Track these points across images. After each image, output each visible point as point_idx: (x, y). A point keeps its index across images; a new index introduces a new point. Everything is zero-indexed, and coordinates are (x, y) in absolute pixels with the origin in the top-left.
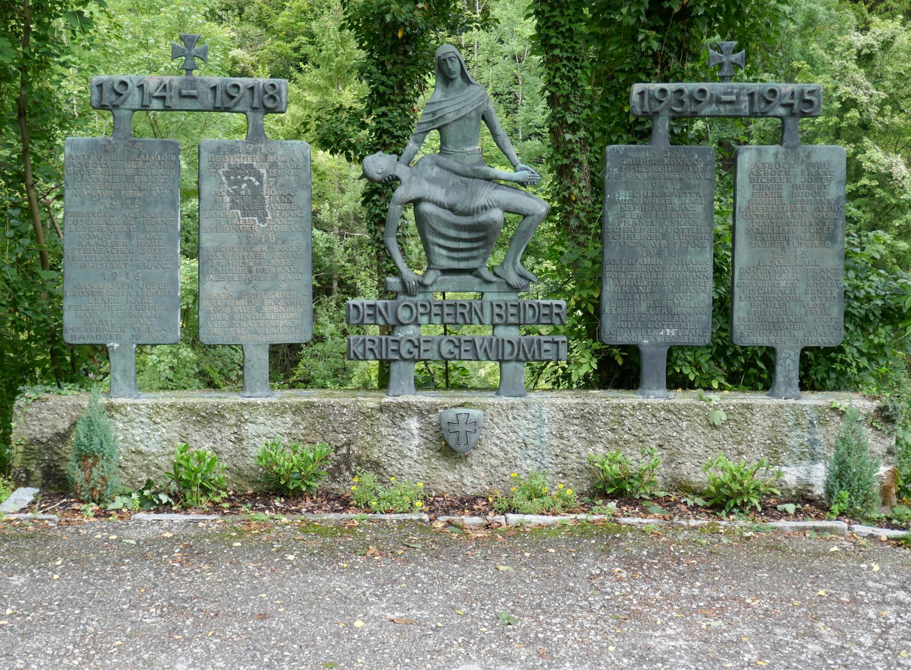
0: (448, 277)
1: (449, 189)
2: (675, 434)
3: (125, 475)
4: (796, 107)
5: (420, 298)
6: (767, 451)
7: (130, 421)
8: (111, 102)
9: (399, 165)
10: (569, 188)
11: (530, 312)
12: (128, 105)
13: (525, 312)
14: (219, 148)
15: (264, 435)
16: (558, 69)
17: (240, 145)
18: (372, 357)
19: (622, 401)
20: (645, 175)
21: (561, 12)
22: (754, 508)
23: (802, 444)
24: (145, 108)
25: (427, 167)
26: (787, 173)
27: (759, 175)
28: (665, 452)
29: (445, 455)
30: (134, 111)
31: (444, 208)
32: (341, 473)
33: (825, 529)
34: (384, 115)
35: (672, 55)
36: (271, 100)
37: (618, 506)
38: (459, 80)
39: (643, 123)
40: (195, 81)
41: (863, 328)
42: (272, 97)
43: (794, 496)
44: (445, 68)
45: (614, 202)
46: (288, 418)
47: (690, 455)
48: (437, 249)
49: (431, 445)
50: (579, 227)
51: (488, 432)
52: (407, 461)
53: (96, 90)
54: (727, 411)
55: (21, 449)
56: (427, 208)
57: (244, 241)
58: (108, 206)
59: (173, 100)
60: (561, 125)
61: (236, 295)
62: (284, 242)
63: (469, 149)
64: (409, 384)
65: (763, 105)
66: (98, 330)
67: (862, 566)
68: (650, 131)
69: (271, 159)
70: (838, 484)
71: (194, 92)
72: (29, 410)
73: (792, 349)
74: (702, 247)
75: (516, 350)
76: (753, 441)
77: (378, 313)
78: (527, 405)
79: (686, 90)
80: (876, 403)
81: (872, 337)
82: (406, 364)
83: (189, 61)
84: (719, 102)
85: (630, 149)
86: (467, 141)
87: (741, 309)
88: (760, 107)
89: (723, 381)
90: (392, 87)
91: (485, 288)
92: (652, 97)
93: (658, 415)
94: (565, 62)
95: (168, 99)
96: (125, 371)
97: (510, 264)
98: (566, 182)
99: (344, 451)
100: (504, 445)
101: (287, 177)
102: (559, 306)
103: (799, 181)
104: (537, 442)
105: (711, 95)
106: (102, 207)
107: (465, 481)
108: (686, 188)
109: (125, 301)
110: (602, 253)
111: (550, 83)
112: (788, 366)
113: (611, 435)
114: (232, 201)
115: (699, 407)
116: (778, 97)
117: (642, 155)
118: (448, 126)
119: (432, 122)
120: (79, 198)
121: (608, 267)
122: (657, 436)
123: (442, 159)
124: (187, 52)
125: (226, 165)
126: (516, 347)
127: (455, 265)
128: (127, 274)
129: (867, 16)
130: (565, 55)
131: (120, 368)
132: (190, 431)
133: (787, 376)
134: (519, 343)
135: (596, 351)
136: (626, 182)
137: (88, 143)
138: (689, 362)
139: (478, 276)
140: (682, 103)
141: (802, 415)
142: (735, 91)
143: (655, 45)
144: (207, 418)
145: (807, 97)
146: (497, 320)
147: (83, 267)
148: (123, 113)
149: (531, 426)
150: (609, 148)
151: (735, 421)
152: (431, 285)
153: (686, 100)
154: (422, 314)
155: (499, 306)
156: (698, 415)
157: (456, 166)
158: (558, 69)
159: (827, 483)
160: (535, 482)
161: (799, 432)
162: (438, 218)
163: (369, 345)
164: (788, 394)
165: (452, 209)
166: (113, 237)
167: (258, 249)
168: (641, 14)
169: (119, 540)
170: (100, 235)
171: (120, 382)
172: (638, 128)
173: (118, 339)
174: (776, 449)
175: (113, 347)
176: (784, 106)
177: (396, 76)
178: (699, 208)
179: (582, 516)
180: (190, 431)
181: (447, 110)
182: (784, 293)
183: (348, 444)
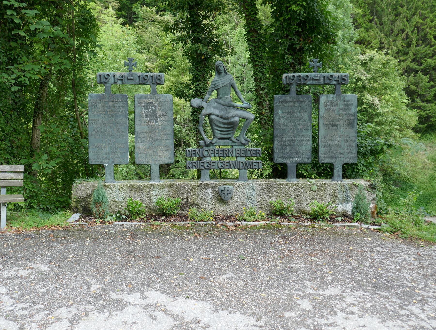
0: (220, 141)
1: (221, 110)
5: (211, 148)
6: (331, 199)
10: (262, 110)
11: (249, 152)
16: (257, 69)
18: (195, 168)
21: (258, 49)
22: (327, 219)
24: (115, 83)
29: (220, 202)
30: (112, 84)
33: (352, 226)
38: (223, 73)
39: (287, 87)
40: (132, 74)
42: (159, 79)
45: (277, 114)
46: (166, 189)
48: (216, 131)
49: (215, 198)
50: (265, 123)
52: (207, 204)
53: (98, 77)
54: (317, 186)
55: (75, 200)
56: (213, 117)
57: (150, 129)
62: (164, 129)
63: (227, 97)
65: (328, 81)
66: (100, 159)
68: (289, 90)
69: (159, 100)
71: (132, 78)
73: (339, 164)
74: (308, 130)
78: (248, 184)
80: (369, 183)
81: (367, 160)
84: (313, 80)
86: (226, 94)
87: (322, 151)
89: (316, 175)
91: (233, 144)
92: (290, 78)
98: (261, 108)
102: (259, 150)
107: (227, 210)
108: (302, 109)
110: (273, 132)
112: (338, 170)
113: (277, 194)
114: (146, 115)
121: (276, 137)
122: (293, 194)
123: (218, 100)
127: (223, 136)
129: (365, 49)
130: (260, 64)
131: (108, 172)
132: (133, 194)
134: (245, 163)
135: (272, 165)
136: (281, 107)
137: (96, 95)
139: (231, 140)
140: (300, 80)
143: (291, 60)
144: (139, 189)
145: (344, 78)
146: (237, 155)
148: (108, 85)
150: (275, 96)
153: (302, 79)
156: (307, 187)
157: (223, 102)
158: (257, 69)
159: (352, 210)
160: (251, 210)
161: (342, 193)
163: (194, 164)
165: (221, 117)
167: (155, 131)
173: (107, 162)
178: (307, 116)
179: (268, 222)
180: (133, 194)
181: (219, 83)
182: (336, 145)
183: (187, 198)
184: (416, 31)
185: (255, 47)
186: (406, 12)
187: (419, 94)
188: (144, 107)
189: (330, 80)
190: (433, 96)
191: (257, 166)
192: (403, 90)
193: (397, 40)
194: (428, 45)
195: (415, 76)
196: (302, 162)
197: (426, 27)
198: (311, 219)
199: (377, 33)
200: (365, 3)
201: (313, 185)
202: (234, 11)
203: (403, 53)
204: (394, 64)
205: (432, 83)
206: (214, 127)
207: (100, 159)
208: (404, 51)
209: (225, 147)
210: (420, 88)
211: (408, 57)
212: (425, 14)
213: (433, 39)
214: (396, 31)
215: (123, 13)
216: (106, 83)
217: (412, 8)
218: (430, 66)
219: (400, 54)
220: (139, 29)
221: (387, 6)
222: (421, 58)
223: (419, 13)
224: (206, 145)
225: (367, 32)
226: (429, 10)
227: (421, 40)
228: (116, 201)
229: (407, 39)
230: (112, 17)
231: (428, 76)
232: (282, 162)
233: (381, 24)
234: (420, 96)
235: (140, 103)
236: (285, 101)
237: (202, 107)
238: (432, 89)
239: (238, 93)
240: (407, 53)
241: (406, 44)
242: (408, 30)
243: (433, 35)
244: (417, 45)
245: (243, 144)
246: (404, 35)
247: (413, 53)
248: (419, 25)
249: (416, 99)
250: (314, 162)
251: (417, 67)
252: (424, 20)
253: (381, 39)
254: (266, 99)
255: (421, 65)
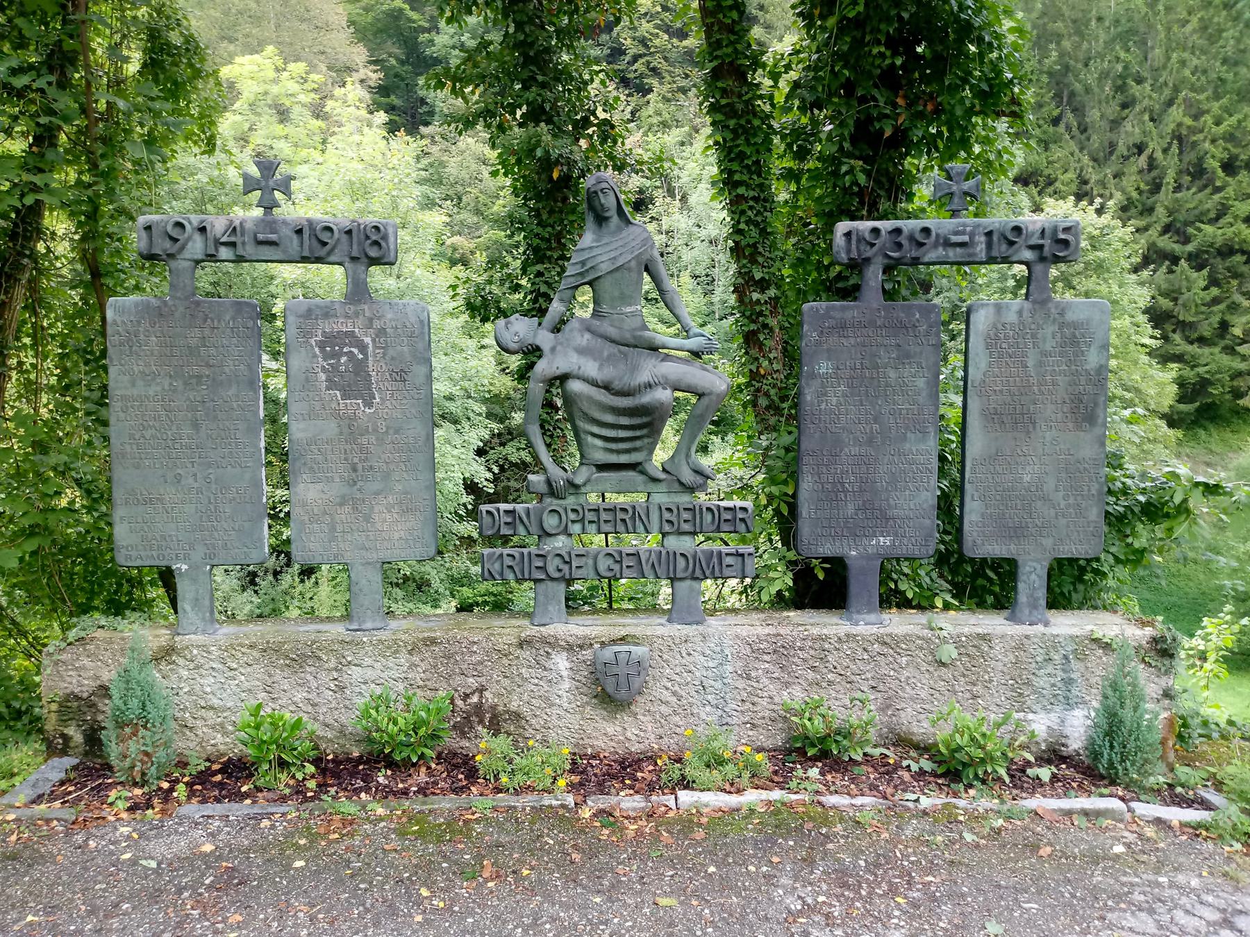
1: (604, 362)
2: (892, 673)
3: (193, 737)
4: (1046, 249)
5: (571, 501)
6: (1009, 694)
7: (197, 667)
8: (165, 251)
9: (540, 332)
10: (757, 359)
11: (708, 517)
12: (187, 254)
13: (701, 518)
14: (309, 311)
15: (373, 682)
16: (743, 212)
17: (337, 306)
19: (825, 631)
20: (852, 341)
21: (747, 140)
22: (999, 779)
23: (1053, 685)
24: (212, 257)
25: (576, 334)
26: (1034, 336)
27: (997, 338)
28: (879, 695)
29: (603, 702)
30: (197, 262)
31: (597, 386)
32: (472, 727)
33: (1099, 814)
34: (539, 274)
35: (882, 193)
36: (376, 248)
37: (822, 774)
38: (615, 219)
39: (847, 279)
40: (275, 222)
41: (1119, 531)
42: (376, 243)
43: (1044, 751)
44: (597, 203)
45: (813, 376)
46: (403, 658)
47: (912, 699)
48: (590, 439)
49: (585, 689)
50: (768, 408)
51: (656, 672)
52: (555, 711)
53: (144, 234)
54: (958, 644)
55: (54, 707)
56: (575, 386)
57: (346, 430)
58: (166, 387)
59: (248, 248)
60: (747, 282)
61: (338, 500)
62: (397, 432)
63: (629, 309)
64: (559, 610)
65: (1004, 247)
66: (159, 547)
67: (1161, 879)
68: (857, 288)
69: (377, 324)
70: (1107, 744)
71: (273, 237)
72: (64, 657)
73: (1037, 561)
74: (924, 433)
75: (691, 565)
76: (991, 681)
77: (518, 521)
78: (704, 638)
79: (905, 229)
80: (1149, 631)
81: (1130, 540)
82: (555, 584)
83: (267, 196)
84: (948, 244)
85: (833, 307)
87: (974, 513)
88: (1001, 249)
89: (948, 598)
90: (548, 240)
91: (652, 487)
92: (861, 239)
93: (870, 648)
94: (751, 203)
95: (239, 246)
96: (197, 600)
97: (683, 456)
98: (754, 352)
99: (475, 699)
100: (677, 688)
101: (399, 348)
102: (744, 509)
103: (1049, 345)
104: (718, 685)
105: (937, 235)
106: (159, 388)
107: (629, 734)
108: (905, 357)
109: (193, 511)
110: (798, 441)
111: (737, 231)
112: (1032, 581)
113: (811, 675)
114: (328, 380)
115: (923, 639)
116: (1023, 236)
117: (848, 315)
118: (602, 280)
119: (581, 274)
120: (127, 378)
121: (805, 460)
123: (596, 323)
124: (263, 184)
125: (320, 332)
126: (691, 561)
128: (195, 475)
129: (1038, 199)
130: (752, 194)
132: (277, 678)
133: (1032, 596)
135: (790, 562)
136: (828, 350)
137: (137, 304)
138: (906, 575)
139: (643, 473)
140: (899, 246)
141: (1054, 647)
142: (968, 229)
143: (862, 179)
145: (1062, 236)
146: (667, 528)
147: (137, 467)
148: (182, 264)
149: (711, 664)
150: (806, 306)
151: (968, 655)
152: (584, 484)
153: (905, 242)
154: (573, 522)
155: (669, 510)
157: (612, 332)
158: (743, 212)
159: (1091, 741)
160: (715, 744)
161: (1050, 669)
162: (590, 399)
163: (508, 561)
164: (1033, 619)
165: (607, 387)
166: (174, 428)
167: (364, 440)
168: (845, 139)
169: (134, 862)
170: (157, 425)
171: (191, 614)
172: (840, 285)
173: (186, 558)
174: (1020, 691)
175: (180, 569)
176: (1031, 247)
177: (553, 227)
178: (921, 383)
179: (776, 795)
180: (277, 678)
183: (481, 690)
184: (1175, 149)
185: (734, 131)
186: (1150, 97)
187: (1179, 322)
188: (322, 348)
189: (1011, 243)
190: (1216, 326)
191: (739, 566)
192: (1144, 313)
193: (1123, 174)
194: (1205, 186)
195: (1171, 271)
196: (902, 551)
197: (1201, 136)
198: (936, 776)
199: (1072, 154)
200: (1041, 72)
201: (944, 641)
202: (690, 94)
203: (1140, 208)
204: (1121, 240)
205: (1215, 291)
206: (581, 424)
207: (159, 547)
208: (1143, 205)
209: (621, 499)
210: (1184, 306)
211: (1154, 219)
212: (1199, 102)
213: (1220, 170)
214: (1122, 149)
215: (394, 100)
216: (171, 256)
217: (1166, 84)
218: (1212, 245)
219: (1133, 211)
220: (434, 142)
221: (1100, 79)
222: (1186, 224)
223: (1184, 100)
224: (553, 491)
225: (1046, 150)
226: (1210, 92)
227: (1189, 174)
228: (212, 708)
229: (1150, 170)
230: (358, 108)
231: (1205, 272)
232: (829, 553)
233: (1083, 129)
234: (1183, 326)
235: (306, 334)
236: (842, 327)
237: (538, 349)
238: (1215, 309)
239: (668, 297)
240: (1150, 210)
241: (1147, 184)
242: (1154, 146)
243: (1221, 161)
244: (1178, 188)
245: (691, 489)
246: (1142, 161)
247: (1167, 208)
248: (1184, 132)
249: (1171, 335)
250: (942, 547)
251: (1177, 248)
252: (1196, 118)
253: (1081, 171)
254: (772, 322)
255: (1186, 240)
